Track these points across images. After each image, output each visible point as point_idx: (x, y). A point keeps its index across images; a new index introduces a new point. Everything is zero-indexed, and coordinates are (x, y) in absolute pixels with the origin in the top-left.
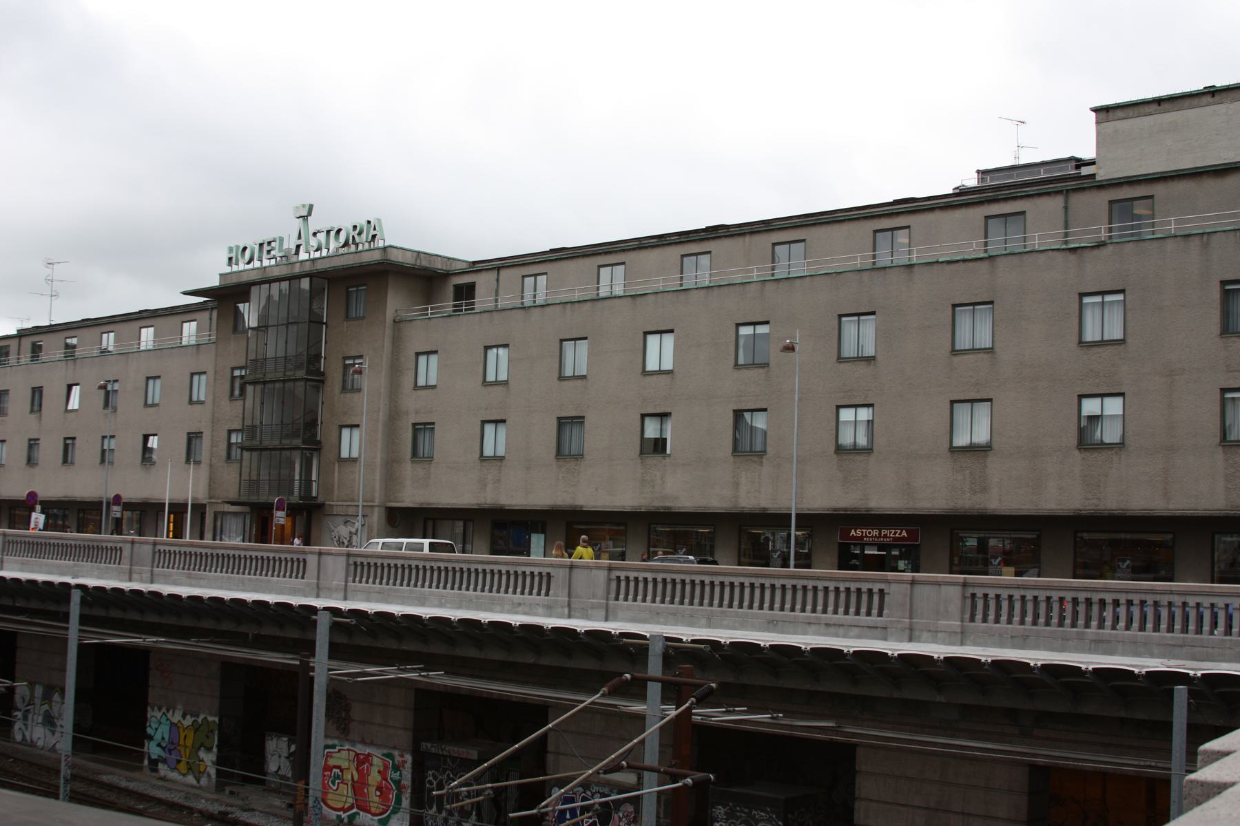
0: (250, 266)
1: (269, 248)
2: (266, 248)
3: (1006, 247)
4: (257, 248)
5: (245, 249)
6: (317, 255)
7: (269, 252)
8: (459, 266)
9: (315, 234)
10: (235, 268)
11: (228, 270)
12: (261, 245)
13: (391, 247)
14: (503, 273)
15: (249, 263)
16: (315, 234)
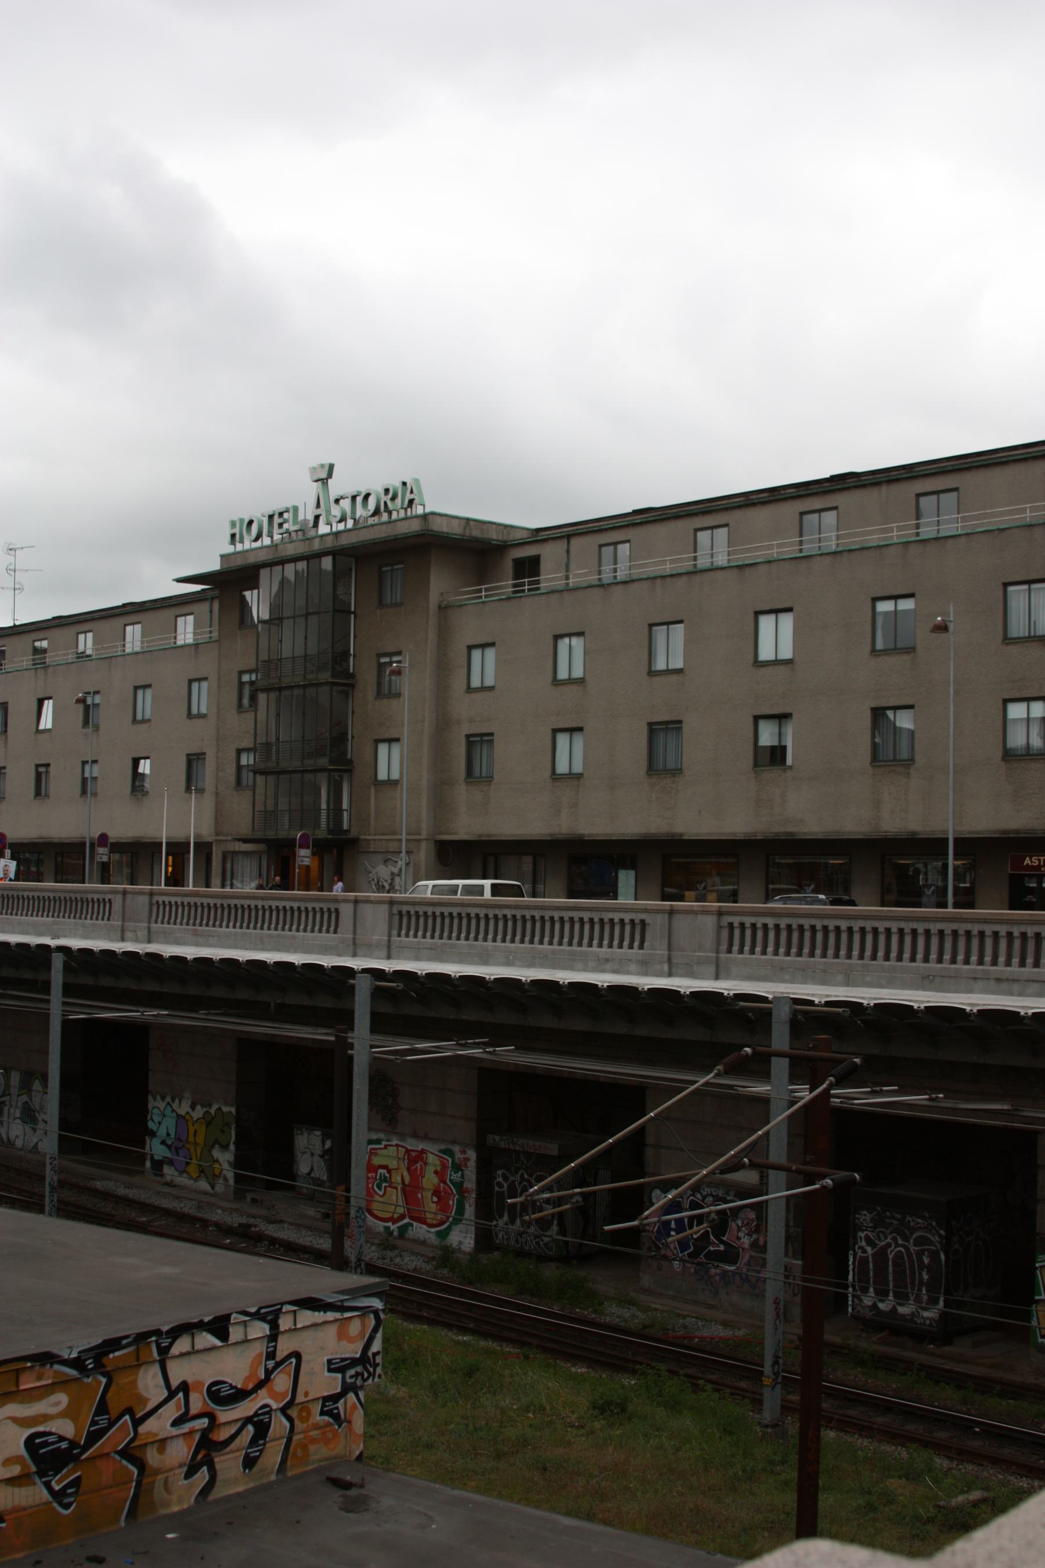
0: (258, 544)
1: (281, 520)
2: (277, 520)
3: (820, 538)
4: (265, 520)
5: (251, 522)
6: (341, 527)
7: (281, 525)
8: (518, 536)
9: (337, 501)
10: (239, 547)
11: (230, 549)
12: (271, 517)
13: (433, 514)
14: (575, 542)
15: (256, 540)
16: (337, 501)
